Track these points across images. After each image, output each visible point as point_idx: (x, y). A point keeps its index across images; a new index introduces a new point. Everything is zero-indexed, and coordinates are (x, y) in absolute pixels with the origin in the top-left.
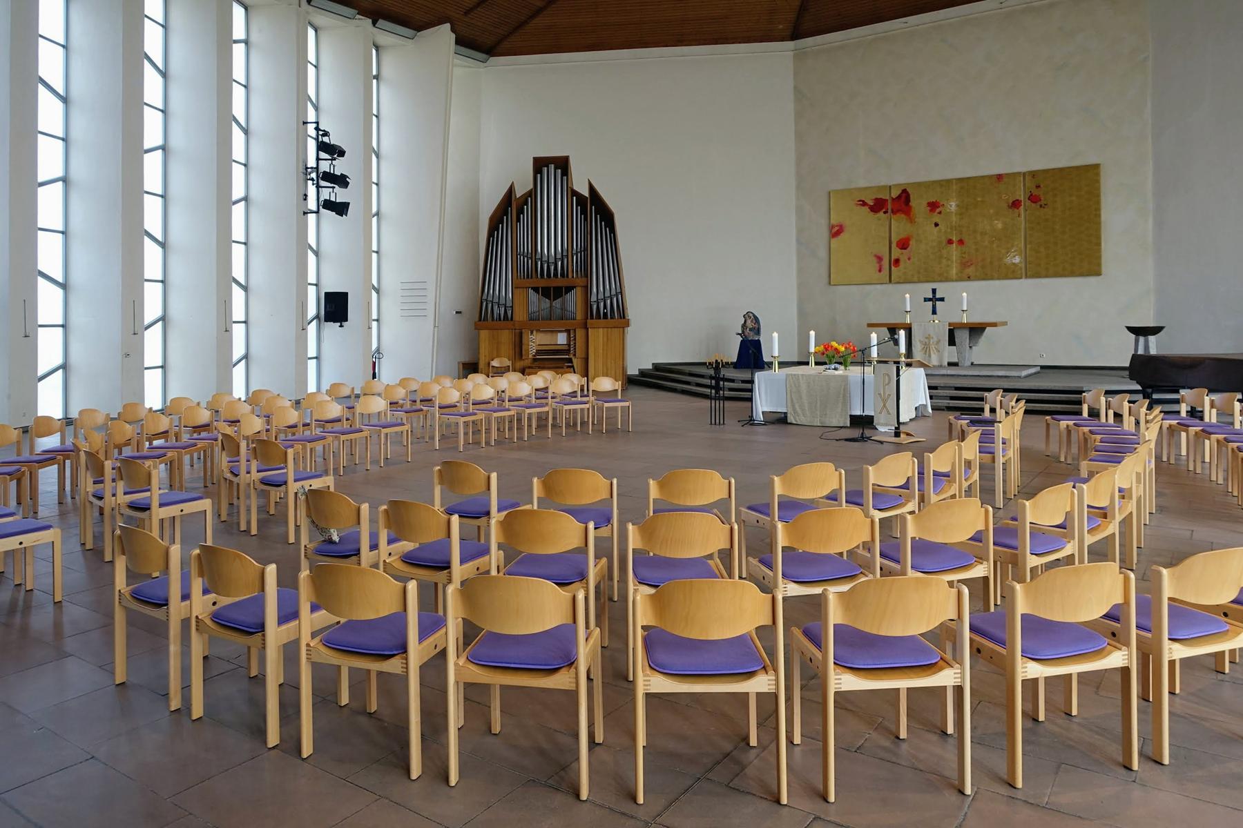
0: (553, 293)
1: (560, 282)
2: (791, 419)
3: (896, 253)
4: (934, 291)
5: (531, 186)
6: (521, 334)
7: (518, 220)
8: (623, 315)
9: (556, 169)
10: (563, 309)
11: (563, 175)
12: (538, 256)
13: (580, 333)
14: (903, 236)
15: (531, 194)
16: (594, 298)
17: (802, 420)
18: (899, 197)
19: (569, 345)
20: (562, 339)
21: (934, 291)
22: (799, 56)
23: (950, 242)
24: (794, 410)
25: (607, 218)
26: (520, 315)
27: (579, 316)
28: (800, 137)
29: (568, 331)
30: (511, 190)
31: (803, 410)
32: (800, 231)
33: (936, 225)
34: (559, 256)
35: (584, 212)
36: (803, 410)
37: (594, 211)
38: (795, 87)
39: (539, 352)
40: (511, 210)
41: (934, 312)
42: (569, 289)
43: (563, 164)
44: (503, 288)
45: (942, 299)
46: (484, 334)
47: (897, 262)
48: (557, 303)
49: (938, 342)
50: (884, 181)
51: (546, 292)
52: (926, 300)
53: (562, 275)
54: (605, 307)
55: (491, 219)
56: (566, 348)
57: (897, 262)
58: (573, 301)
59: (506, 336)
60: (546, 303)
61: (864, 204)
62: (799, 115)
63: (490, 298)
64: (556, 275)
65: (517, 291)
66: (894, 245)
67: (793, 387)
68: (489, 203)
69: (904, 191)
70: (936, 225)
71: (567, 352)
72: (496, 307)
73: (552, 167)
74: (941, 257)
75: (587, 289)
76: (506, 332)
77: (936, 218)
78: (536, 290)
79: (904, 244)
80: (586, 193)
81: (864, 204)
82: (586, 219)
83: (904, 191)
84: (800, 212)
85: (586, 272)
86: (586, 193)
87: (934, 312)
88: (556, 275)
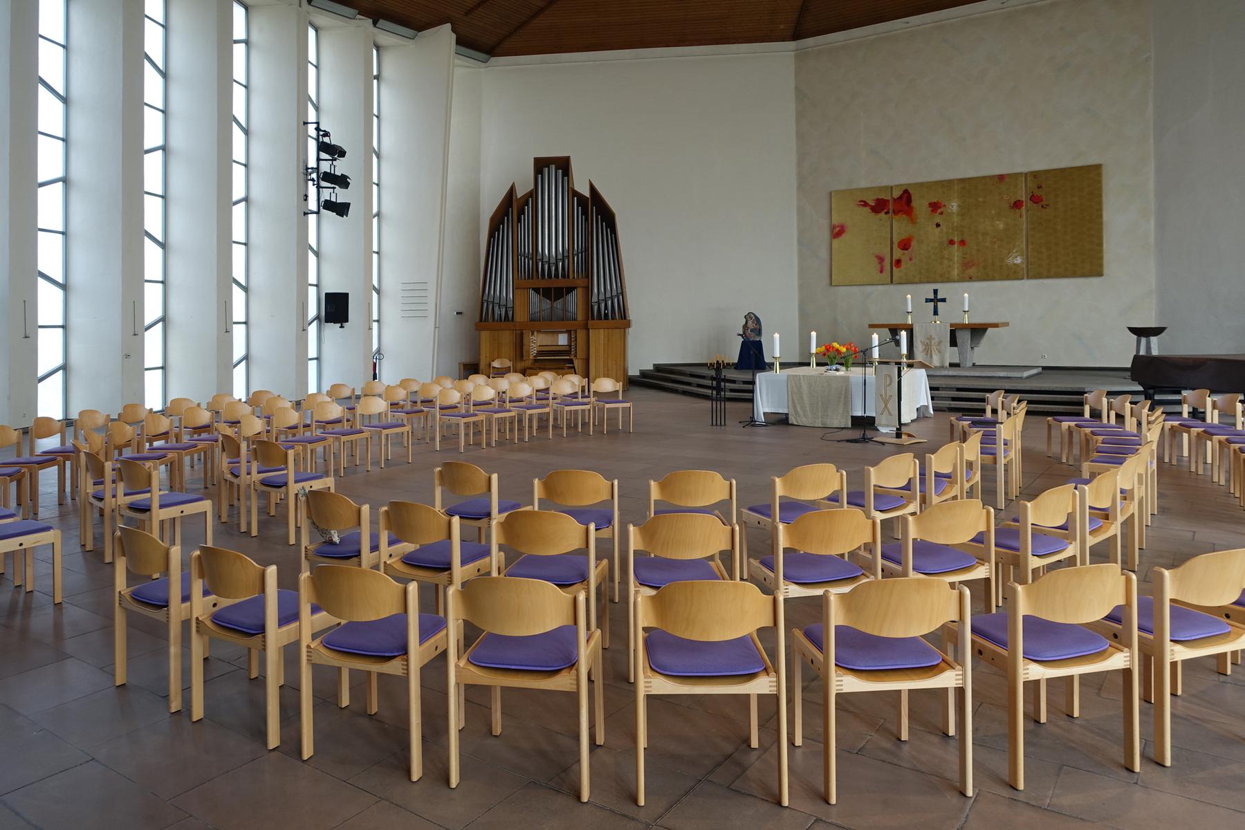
0: (554, 293)
1: (561, 283)
2: (792, 420)
3: (898, 253)
4: (936, 292)
5: (532, 187)
6: (522, 334)
7: (519, 221)
8: (624, 315)
9: (556, 169)
10: (565, 310)
11: (563, 176)
12: (539, 257)
13: (581, 334)
14: (904, 236)
15: (532, 195)
16: (595, 299)
17: (804, 421)
18: (900, 198)
19: (570, 346)
20: (563, 340)
21: (936, 292)
22: (800, 56)
23: (952, 242)
24: (796, 411)
25: (608, 219)
26: (521, 316)
27: (580, 317)
28: (801, 137)
29: (569, 332)
30: (512, 191)
31: (804, 411)
32: (801, 233)
33: (938, 225)
34: (560, 257)
35: (585, 212)
36: (804, 411)
37: (595, 213)
38: (797, 88)
39: (540, 353)
40: (512, 211)
41: (936, 313)
42: (570, 290)
43: (564, 165)
44: (504, 289)
45: (944, 300)
46: (485, 335)
47: (898, 262)
48: (559, 304)
49: (940, 343)
50: (885, 181)
51: (547, 293)
52: (927, 300)
53: (563, 276)
54: (606, 308)
55: (492, 220)
56: (567, 348)
57: (898, 262)
58: (574, 302)
59: (507, 337)
60: (546, 304)
61: (865, 204)
62: (800, 115)
63: (491, 299)
64: (557, 276)
65: (518, 292)
66: (895, 246)
67: (794, 388)
68: (490, 204)
69: (906, 192)
70: (938, 225)
71: (568, 352)
72: (496, 308)
73: (553, 167)
74: (943, 257)
75: (588, 290)
76: (507, 332)
77: (938, 219)
78: (537, 290)
79: (905, 245)
80: (587, 193)
81: (865, 204)
82: (587, 220)
83: (906, 192)
84: (800, 210)
85: (588, 274)
86: (587, 193)
87: (936, 313)
88: (557, 276)
